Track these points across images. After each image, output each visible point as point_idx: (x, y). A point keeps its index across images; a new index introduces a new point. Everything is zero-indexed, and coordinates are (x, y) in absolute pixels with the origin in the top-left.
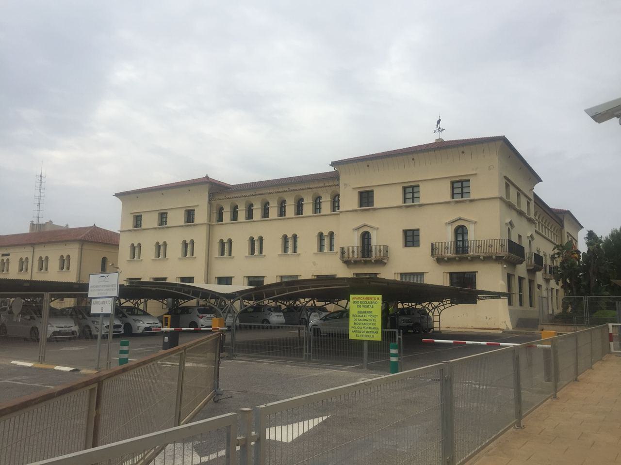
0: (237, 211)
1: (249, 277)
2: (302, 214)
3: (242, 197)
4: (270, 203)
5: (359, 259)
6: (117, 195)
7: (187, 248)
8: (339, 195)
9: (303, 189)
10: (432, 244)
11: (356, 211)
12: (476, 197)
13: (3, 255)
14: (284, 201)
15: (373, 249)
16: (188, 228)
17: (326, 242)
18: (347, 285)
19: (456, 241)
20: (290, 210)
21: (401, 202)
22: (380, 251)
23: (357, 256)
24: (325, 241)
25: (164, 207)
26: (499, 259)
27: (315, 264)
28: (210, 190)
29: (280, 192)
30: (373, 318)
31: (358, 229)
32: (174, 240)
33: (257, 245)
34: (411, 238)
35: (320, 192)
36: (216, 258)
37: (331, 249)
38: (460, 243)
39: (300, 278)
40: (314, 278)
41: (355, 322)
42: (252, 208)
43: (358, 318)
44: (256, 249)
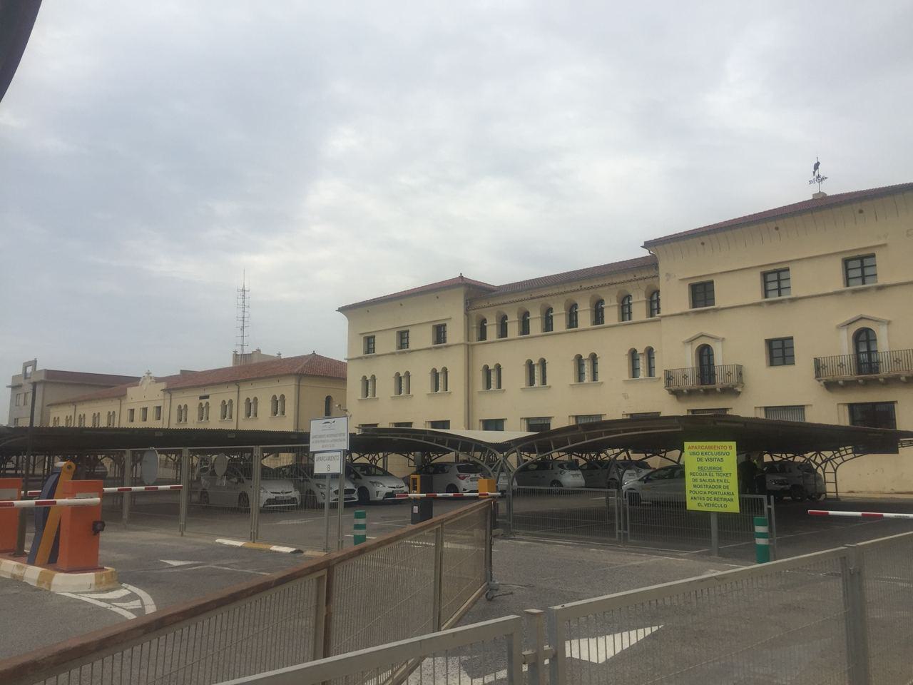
0: (486, 327)
1: (528, 419)
5: (696, 387)
7: (439, 379)
8: (577, 304)
10: (817, 361)
11: (686, 314)
13: (201, 398)
17: (642, 364)
18: (677, 427)
19: (858, 353)
20: (585, 318)
27: (626, 397)
29: (568, 292)
30: (723, 478)
31: (691, 341)
32: (420, 367)
34: (780, 352)
35: (602, 293)
39: (604, 419)
40: (625, 417)
41: (695, 483)
42: (528, 318)
43: (699, 477)
44: (536, 377)
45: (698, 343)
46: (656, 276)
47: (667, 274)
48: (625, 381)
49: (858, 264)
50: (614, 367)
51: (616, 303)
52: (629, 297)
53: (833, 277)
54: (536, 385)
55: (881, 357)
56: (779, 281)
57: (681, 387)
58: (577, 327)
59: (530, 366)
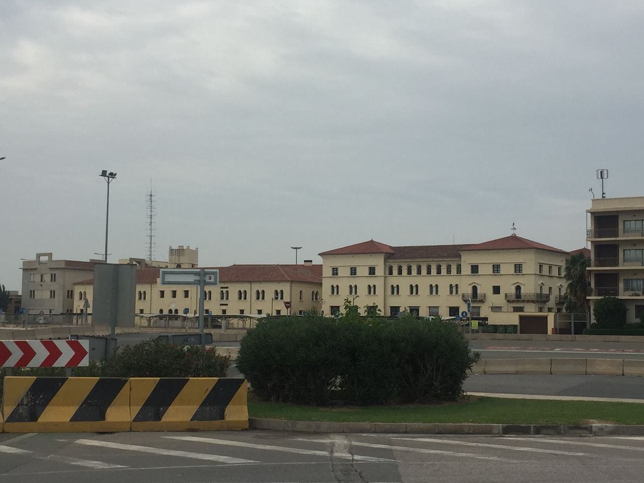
3: (405, 262)
6: (319, 254)
7: (371, 289)
9: (441, 261)
10: (506, 294)
11: (349, 277)
13: (221, 288)
14: (440, 266)
15: (478, 295)
19: (517, 293)
21: (436, 273)
26: (533, 302)
27: (448, 300)
28: (385, 256)
32: (362, 285)
33: (414, 289)
34: (496, 290)
35: (440, 263)
36: (389, 296)
37: (457, 293)
45: (516, 285)
46: (461, 260)
47: (464, 261)
48: (448, 296)
50: (444, 290)
51: (445, 267)
52: (450, 266)
54: (454, 294)
55: (522, 295)
56: (519, 267)
57: (529, 299)
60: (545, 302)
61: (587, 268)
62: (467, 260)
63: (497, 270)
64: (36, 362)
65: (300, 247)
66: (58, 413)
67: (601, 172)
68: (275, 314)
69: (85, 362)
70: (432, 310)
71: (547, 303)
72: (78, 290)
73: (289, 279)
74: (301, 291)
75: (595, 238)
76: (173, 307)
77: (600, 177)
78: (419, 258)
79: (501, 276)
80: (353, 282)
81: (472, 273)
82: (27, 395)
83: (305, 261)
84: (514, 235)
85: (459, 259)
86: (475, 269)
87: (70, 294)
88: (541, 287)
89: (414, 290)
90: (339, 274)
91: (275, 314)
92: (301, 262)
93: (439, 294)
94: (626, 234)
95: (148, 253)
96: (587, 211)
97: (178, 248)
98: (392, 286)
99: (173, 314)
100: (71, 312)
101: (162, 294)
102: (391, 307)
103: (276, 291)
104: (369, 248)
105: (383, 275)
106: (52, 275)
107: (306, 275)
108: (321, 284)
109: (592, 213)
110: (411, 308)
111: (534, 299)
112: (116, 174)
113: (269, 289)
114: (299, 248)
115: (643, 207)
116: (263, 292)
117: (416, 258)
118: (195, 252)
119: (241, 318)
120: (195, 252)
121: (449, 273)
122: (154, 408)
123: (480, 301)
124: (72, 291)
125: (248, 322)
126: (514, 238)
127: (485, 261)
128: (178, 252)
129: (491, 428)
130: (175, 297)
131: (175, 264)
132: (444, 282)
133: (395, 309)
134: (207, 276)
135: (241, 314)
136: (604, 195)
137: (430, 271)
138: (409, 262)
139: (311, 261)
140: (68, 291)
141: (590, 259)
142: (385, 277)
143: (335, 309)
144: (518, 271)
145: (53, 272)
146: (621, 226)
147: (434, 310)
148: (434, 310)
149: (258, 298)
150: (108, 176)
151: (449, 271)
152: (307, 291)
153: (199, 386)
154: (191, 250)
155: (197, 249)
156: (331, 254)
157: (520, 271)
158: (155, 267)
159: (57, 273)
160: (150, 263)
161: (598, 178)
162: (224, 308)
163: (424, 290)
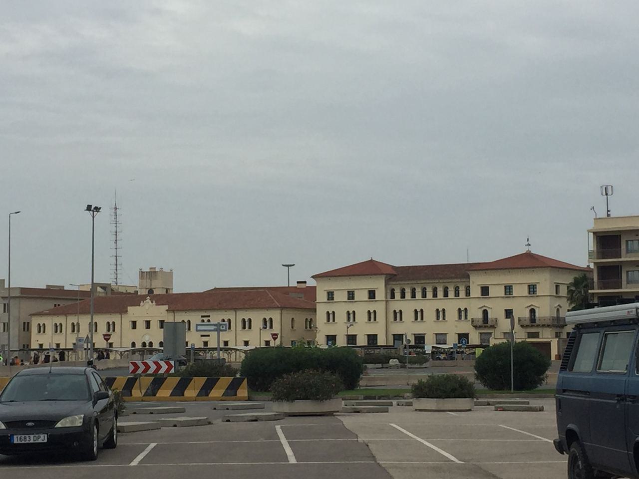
1: (414, 334)
2: (448, 297)
3: (408, 284)
4: (449, 288)
5: (528, 324)
6: (313, 277)
7: (372, 316)
10: (519, 318)
12: (491, 296)
13: (202, 317)
16: (507, 299)
17: (463, 314)
19: (531, 317)
20: (419, 295)
22: (493, 321)
23: (480, 323)
24: (462, 313)
25: (331, 288)
26: (548, 326)
27: (456, 326)
31: (528, 307)
34: (509, 313)
35: (436, 285)
36: (392, 322)
37: (466, 318)
38: (533, 317)
45: (530, 308)
46: (469, 282)
49: (532, 287)
50: (452, 315)
51: (442, 290)
53: (525, 292)
58: (488, 295)
59: (348, 313)
60: (563, 326)
61: (590, 291)
62: (476, 282)
63: (510, 292)
64: (150, 371)
65: (292, 264)
66: (164, 392)
67: (606, 188)
68: (263, 345)
69: (172, 371)
70: (439, 337)
71: (565, 327)
72: (35, 322)
73: (279, 306)
74: (293, 319)
75: (597, 259)
76: (147, 340)
77: (604, 193)
78: (423, 279)
79: (514, 299)
80: (351, 307)
81: (482, 295)
82: (150, 385)
83: (298, 282)
84: (528, 252)
85: (468, 280)
86: (485, 291)
87: (27, 327)
88: (558, 310)
89: (419, 315)
90: (335, 298)
91: (263, 345)
92: (293, 284)
93: (446, 320)
94: (628, 255)
95: (113, 276)
96: (589, 231)
97: (149, 271)
98: (395, 311)
99: (147, 347)
100: (28, 347)
101: (134, 324)
102: (394, 335)
103: (265, 319)
104: (369, 269)
105: (384, 299)
106: (5, 305)
107: (297, 300)
108: (315, 310)
109: (594, 233)
110: (416, 336)
111: (549, 323)
112: (100, 208)
113: (257, 317)
114: (291, 266)
115: (638, 227)
116: (250, 320)
117: (420, 279)
118: (170, 274)
119: (225, 350)
120: (170, 274)
121: (468, 295)
122: (205, 390)
123: (491, 326)
124: (28, 323)
125: (233, 355)
126: (529, 255)
127: (496, 282)
128: (152, 274)
129: (358, 397)
130: (136, 328)
131: (146, 289)
132: (451, 306)
133: (398, 337)
134: (221, 327)
135: (204, 346)
136: (609, 213)
137: (437, 294)
138: (412, 284)
139: (305, 282)
140: (24, 323)
141: (593, 282)
142: (387, 301)
143: (331, 338)
144: (532, 292)
145: (6, 302)
146: (623, 247)
147: (441, 338)
148: (441, 338)
149: (244, 327)
150: (93, 211)
151: (457, 294)
152: (300, 318)
153: (225, 381)
154: (164, 272)
155: (171, 270)
156: (327, 277)
157: (534, 292)
158: (130, 293)
159: (13, 303)
160: (117, 287)
161: (602, 194)
162: (205, 339)
163: (430, 315)
